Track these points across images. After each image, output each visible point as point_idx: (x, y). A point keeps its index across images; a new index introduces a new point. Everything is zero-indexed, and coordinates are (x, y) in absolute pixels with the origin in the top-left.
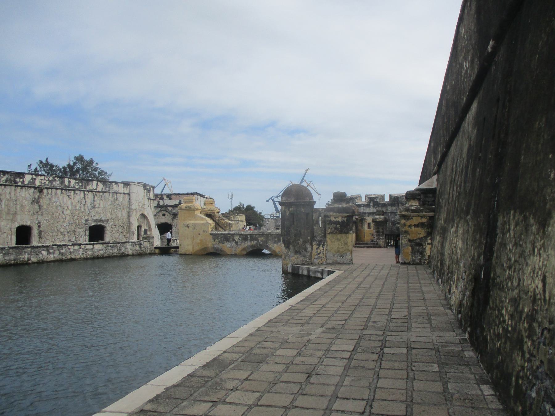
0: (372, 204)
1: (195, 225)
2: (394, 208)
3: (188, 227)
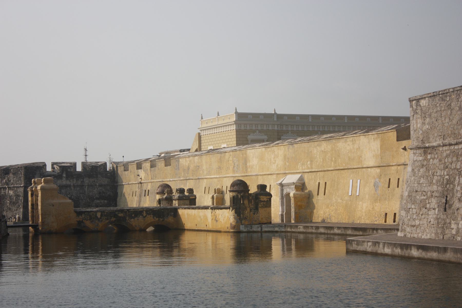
0: (64, 175)
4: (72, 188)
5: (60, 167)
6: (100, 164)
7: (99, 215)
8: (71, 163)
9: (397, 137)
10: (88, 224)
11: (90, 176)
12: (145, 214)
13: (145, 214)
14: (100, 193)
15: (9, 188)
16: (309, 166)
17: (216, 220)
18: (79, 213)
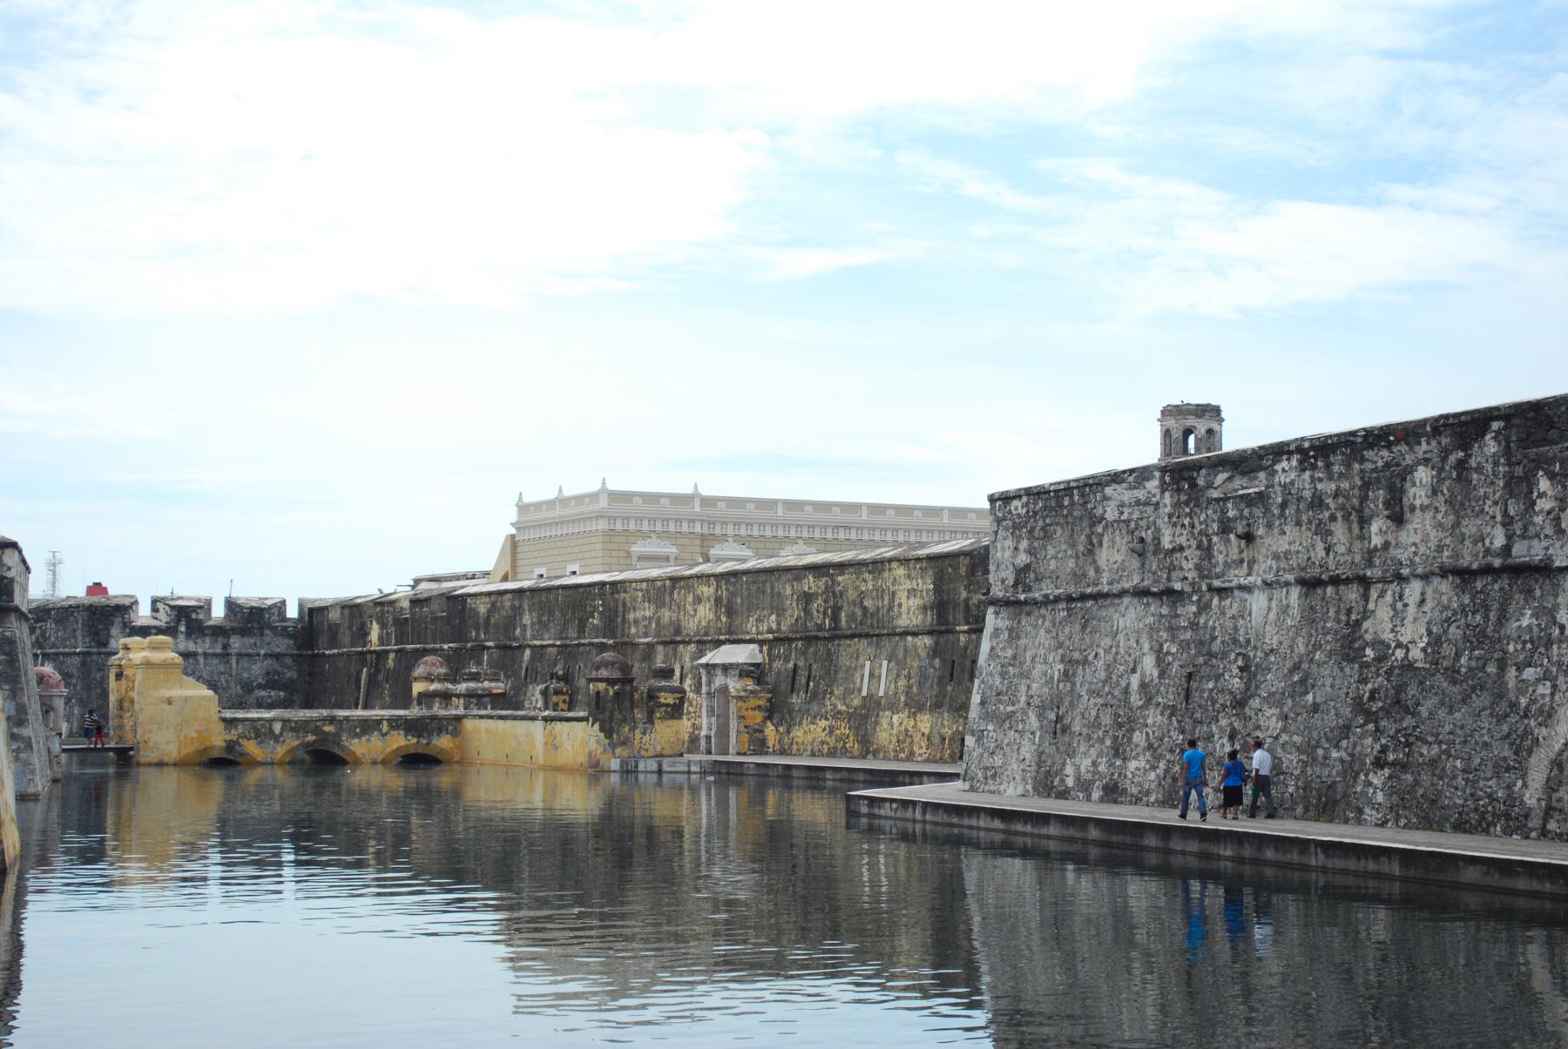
0: (183, 629)
1: (186, 699)
2: (248, 641)
3: (170, 703)
4: (201, 659)
5: (172, 607)
6: (269, 603)
7: (277, 727)
8: (198, 600)
9: (209, 610)
10: (252, 748)
11: (243, 632)
12: (385, 727)
13: (385, 727)
14: (268, 673)
15: (44, 655)
16: (774, 626)
17: (553, 745)
18: (230, 723)
